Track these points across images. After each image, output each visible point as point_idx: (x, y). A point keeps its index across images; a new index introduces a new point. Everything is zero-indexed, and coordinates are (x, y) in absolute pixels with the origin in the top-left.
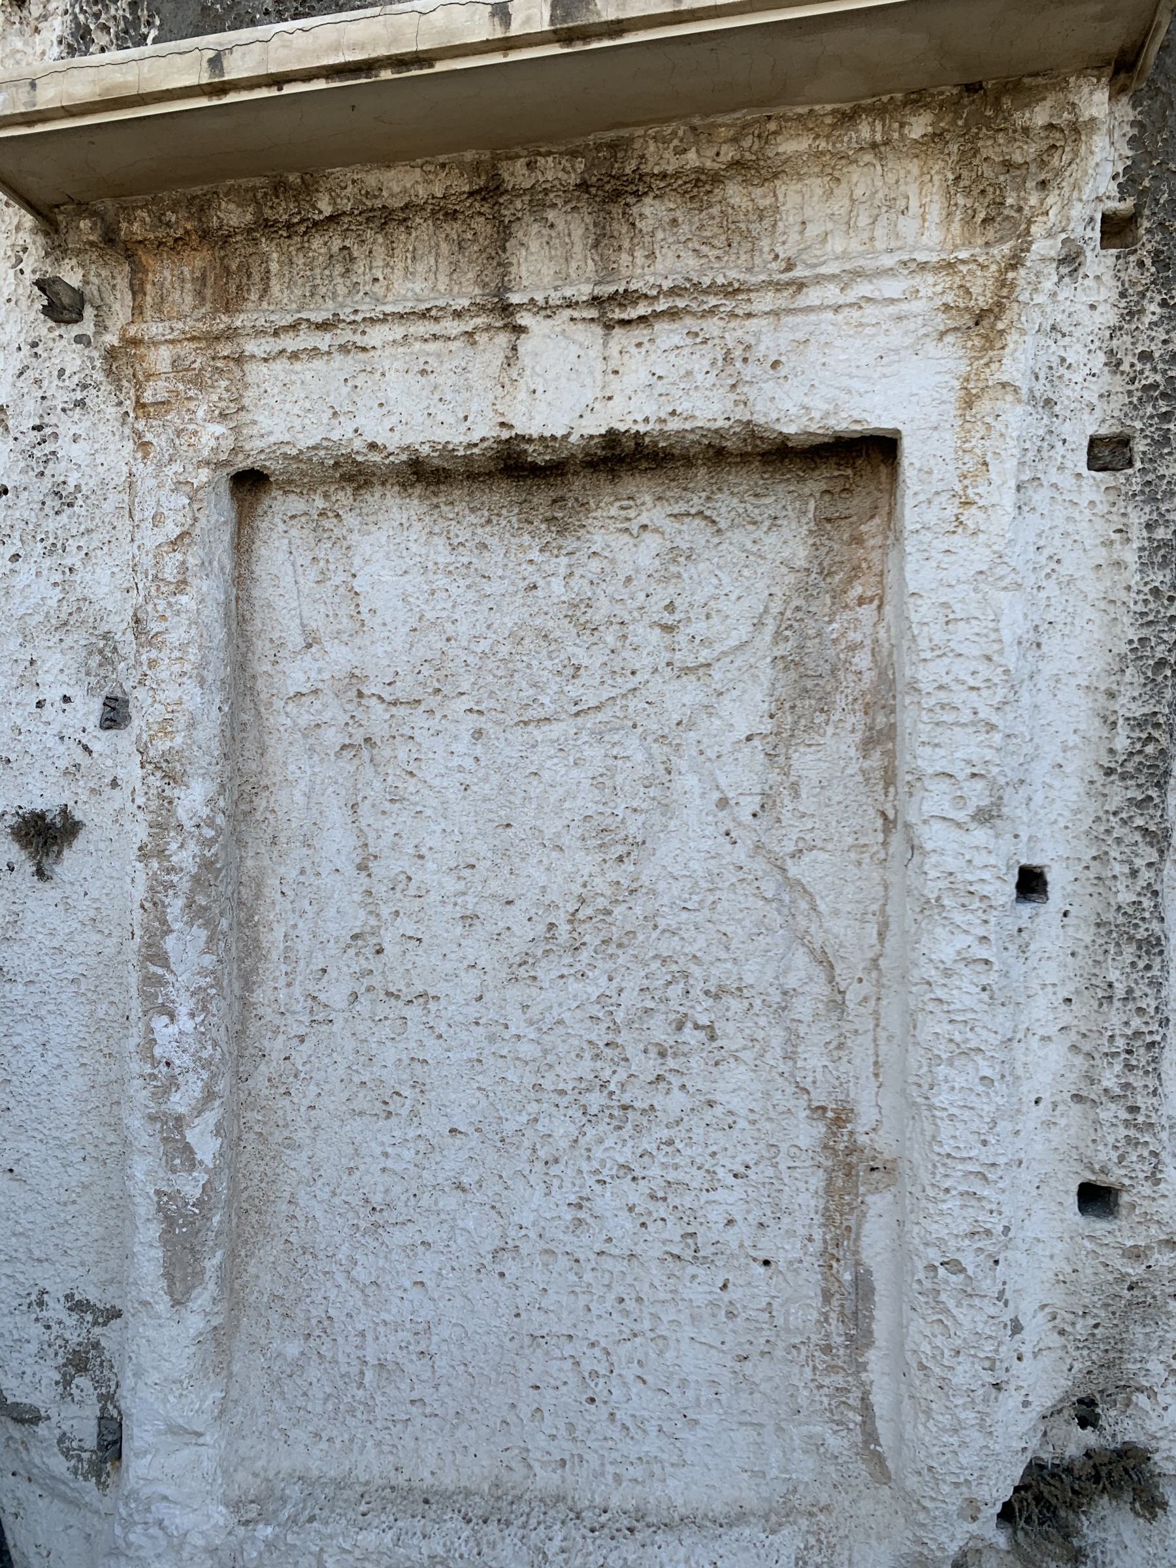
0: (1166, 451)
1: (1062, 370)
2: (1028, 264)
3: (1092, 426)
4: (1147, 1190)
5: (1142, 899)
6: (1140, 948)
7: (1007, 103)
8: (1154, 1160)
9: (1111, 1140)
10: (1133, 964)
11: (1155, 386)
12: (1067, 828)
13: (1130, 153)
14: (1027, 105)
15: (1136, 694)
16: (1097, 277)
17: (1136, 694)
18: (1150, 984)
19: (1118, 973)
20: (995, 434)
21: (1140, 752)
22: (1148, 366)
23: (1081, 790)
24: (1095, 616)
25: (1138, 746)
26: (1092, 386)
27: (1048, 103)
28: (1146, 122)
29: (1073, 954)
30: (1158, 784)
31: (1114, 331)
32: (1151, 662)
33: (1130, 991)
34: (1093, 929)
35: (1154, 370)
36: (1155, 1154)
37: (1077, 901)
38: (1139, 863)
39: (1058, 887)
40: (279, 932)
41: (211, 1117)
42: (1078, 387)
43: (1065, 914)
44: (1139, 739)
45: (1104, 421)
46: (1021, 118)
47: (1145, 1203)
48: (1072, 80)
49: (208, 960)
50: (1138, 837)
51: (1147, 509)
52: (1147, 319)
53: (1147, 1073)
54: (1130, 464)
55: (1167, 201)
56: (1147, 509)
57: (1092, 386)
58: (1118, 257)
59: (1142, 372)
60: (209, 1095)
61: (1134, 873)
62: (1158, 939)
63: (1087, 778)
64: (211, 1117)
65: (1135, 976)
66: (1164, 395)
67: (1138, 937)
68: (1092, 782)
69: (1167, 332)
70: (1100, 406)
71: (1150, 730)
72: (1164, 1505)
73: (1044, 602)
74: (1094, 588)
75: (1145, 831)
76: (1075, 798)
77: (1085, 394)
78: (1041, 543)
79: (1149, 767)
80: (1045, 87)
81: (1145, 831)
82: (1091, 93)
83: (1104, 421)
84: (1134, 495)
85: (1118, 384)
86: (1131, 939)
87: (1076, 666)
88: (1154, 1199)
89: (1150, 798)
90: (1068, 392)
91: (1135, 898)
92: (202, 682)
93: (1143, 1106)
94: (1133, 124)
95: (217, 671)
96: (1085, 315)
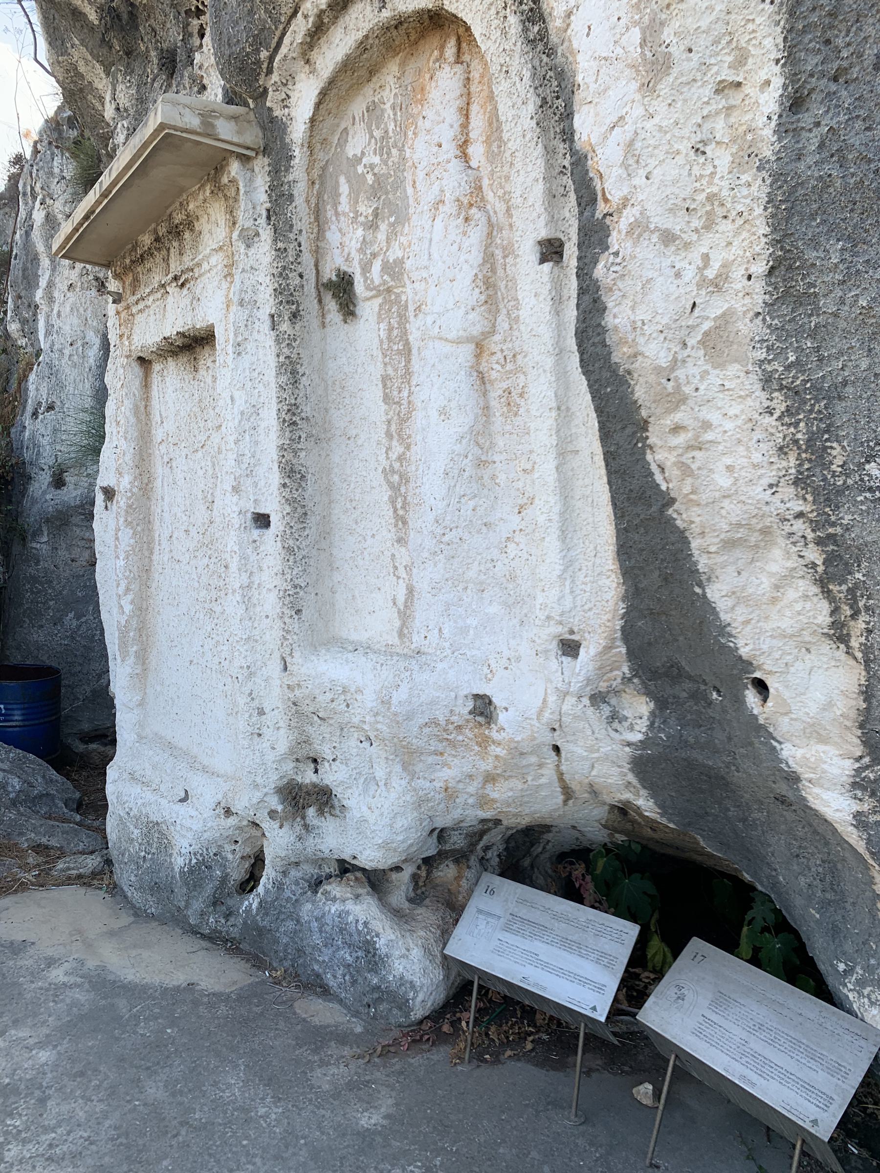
30: (289, 476)
40: (158, 533)
41: (130, 597)
49: (132, 541)
60: (128, 590)
64: (130, 597)
72: (279, 791)
73: (257, 395)
92: (126, 438)
94: (269, 165)
95: (133, 433)
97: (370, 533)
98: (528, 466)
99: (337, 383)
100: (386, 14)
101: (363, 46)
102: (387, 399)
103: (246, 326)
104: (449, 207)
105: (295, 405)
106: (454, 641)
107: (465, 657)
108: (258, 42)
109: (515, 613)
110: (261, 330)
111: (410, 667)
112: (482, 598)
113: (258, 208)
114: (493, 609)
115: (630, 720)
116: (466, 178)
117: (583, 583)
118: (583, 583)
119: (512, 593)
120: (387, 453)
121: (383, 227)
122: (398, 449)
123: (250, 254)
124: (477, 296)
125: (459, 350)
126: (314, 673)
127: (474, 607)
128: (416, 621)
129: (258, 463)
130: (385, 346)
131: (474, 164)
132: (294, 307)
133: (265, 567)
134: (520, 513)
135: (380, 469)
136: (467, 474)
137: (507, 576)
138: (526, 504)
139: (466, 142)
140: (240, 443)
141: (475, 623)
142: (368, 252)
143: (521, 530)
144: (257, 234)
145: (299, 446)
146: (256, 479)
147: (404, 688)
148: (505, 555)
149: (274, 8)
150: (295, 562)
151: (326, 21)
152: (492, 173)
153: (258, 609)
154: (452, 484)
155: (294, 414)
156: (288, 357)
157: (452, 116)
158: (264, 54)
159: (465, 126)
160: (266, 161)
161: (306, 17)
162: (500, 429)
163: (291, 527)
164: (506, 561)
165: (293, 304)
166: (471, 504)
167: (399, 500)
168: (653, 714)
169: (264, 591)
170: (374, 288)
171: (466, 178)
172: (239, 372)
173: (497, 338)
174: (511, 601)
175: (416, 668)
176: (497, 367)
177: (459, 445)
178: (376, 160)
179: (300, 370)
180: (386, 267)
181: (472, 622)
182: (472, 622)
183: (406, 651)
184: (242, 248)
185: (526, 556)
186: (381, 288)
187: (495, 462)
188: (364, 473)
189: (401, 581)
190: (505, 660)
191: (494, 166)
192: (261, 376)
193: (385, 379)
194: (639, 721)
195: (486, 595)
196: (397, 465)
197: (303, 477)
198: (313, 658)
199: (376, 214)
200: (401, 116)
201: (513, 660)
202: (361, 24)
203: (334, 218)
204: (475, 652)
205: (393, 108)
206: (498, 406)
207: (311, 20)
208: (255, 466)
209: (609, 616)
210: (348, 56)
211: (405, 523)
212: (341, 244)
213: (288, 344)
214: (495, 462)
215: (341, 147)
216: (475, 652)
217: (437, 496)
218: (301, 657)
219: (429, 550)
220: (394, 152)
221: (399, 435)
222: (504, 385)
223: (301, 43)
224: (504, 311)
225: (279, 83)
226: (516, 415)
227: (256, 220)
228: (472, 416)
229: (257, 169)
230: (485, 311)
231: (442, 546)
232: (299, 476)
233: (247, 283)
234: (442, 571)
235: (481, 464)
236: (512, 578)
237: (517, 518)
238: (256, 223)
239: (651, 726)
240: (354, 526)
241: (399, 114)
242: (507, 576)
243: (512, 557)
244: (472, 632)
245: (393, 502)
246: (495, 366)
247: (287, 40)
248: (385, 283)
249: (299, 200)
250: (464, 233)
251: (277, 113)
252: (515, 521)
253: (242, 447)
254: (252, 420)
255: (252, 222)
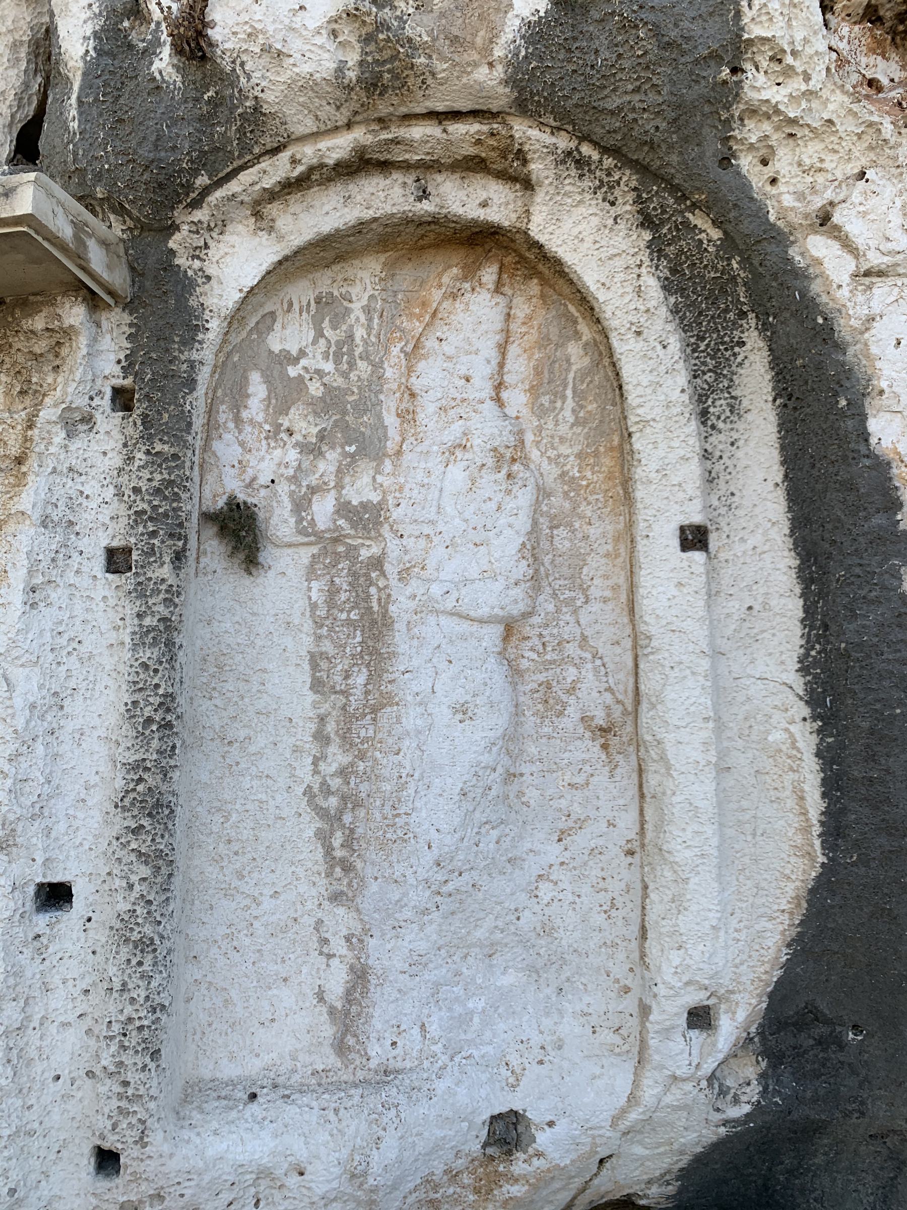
0: (152, 559)
1: (80, 500)
2: (39, 425)
3: (104, 540)
4: (135, 1152)
5: (137, 908)
6: (136, 947)
7: (18, 313)
8: (141, 1127)
9: (106, 1110)
10: (129, 961)
11: (144, 512)
12: (91, 849)
13: (129, 346)
14: (30, 315)
15: (130, 745)
16: (107, 432)
17: (130, 745)
18: (142, 977)
19: (115, 969)
20: (13, 550)
21: (134, 790)
22: (139, 498)
23: (100, 819)
24: (110, 683)
25: (132, 786)
26: (105, 511)
27: (43, 314)
28: (141, 323)
29: (94, 953)
30: (150, 815)
31: (120, 470)
32: (141, 720)
33: (124, 984)
34: (107, 932)
35: (143, 500)
36: (142, 1122)
37: (98, 909)
38: (134, 878)
39: (82, 898)
42: (93, 512)
43: (89, 920)
44: (133, 780)
45: (114, 536)
46: (27, 324)
47: (134, 1164)
48: (59, 298)
50: (133, 857)
51: (138, 603)
52: (137, 463)
53: (137, 1052)
54: (131, 568)
55: (150, 380)
56: (138, 603)
57: (105, 511)
58: (123, 419)
59: (135, 501)
61: (131, 887)
62: (152, 939)
63: (104, 810)
65: (128, 971)
66: (151, 519)
67: (133, 939)
68: (107, 813)
69: (151, 473)
70: (112, 525)
71: (141, 773)
73: (64, 674)
74: (108, 662)
75: (140, 854)
76: (96, 825)
77: (100, 517)
78: (61, 629)
79: (141, 802)
80: (42, 302)
81: (140, 854)
82: (71, 308)
83: (114, 536)
84: (130, 593)
85: (122, 510)
86: (127, 940)
87: (97, 722)
88: (142, 1160)
89: (142, 826)
90: (86, 516)
91: (129, 907)
93: (132, 1081)
94: (131, 325)
96: (99, 460)
97: (268, 891)
98: (580, 779)
99: (211, 659)
100: (427, 206)
101: (361, 227)
102: (317, 685)
103: (53, 560)
104: (479, 453)
105: (171, 695)
106: (449, 1040)
107: (473, 1061)
108: (201, 162)
109: (547, 979)
110: (84, 569)
111: (391, 1101)
112: (491, 966)
113: (99, 382)
114: (507, 980)
115: (733, 1091)
116: (510, 428)
117: (736, 930)
118: (736, 930)
119: (542, 951)
120: (315, 763)
121: (332, 456)
122: (337, 757)
123: (72, 448)
124: (522, 569)
125: (484, 631)
126: (201, 1164)
127: (479, 981)
128: (374, 1021)
129: (57, 792)
130: (322, 612)
131: (511, 411)
132: (180, 543)
133: (56, 980)
134: (560, 840)
135: (300, 790)
136: (493, 793)
137: (538, 929)
138: (571, 829)
139: (500, 384)
140: (21, 759)
141: (481, 1005)
142: (304, 484)
143: (562, 864)
144: (88, 420)
145: (172, 763)
146: (49, 822)
147: (390, 1141)
148: (536, 900)
149: (251, 132)
150: (155, 964)
151: (314, 177)
152: (540, 429)
153: (38, 1067)
154: (471, 809)
155: (168, 710)
156: (163, 620)
157: (488, 348)
158: (202, 180)
159: (501, 365)
160: (127, 318)
161: (294, 161)
162: (533, 732)
163: (149, 902)
164: (537, 908)
165: (179, 539)
166: (495, 834)
167: (339, 834)
168: (763, 1076)
169: (53, 1029)
170: (315, 534)
171: (510, 428)
172: (30, 636)
173: (536, 620)
174: (540, 963)
175: (402, 1099)
176: (534, 656)
177: (487, 755)
178: (329, 367)
179: (177, 640)
180: (344, 509)
181: (476, 1004)
182: (476, 1004)
183: (360, 1075)
184: (59, 436)
185: (571, 898)
186: (327, 535)
187: (522, 775)
188: (263, 797)
189: (335, 962)
190: (536, 1050)
191: (542, 421)
192: (75, 645)
193: (315, 660)
194: (748, 1090)
195: (497, 960)
196: (335, 783)
197: (172, 811)
198: (186, 1134)
199: (321, 436)
200: (380, 325)
201: (549, 1048)
202: (376, 203)
203: (231, 425)
204: (485, 1049)
205: (367, 310)
206: (530, 702)
207: (300, 169)
208: (50, 797)
209: (767, 967)
210: (337, 230)
211: (348, 868)
212: (240, 462)
213: (165, 600)
214: (522, 775)
215: (260, 334)
216: (485, 1049)
217: (444, 827)
218: (165, 1139)
219: (415, 907)
220: (362, 365)
221: (344, 738)
222: (541, 677)
223: (264, 189)
224: (548, 590)
225: (205, 226)
226: (560, 714)
227: (91, 399)
228: (506, 716)
229: (105, 325)
230: (529, 588)
231: (438, 898)
232: (167, 812)
233: (59, 492)
234: (434, 937)
235: (511, 776)
236: (547, 930)
237: (557, 848)
238: (94, 404)
239: (764, 1092)
240: (235, 883)
241: (376, 321)
242: (538, 929)
243: (545, 902)
244: (476, 1020)
245: (324, 837)
246: (528, 654)
247: (245, 177)
248: (338, 528)
249: (201, 390)
250: (509, 492)
251: (181, 261)
252: (553, 852)
253: (24, 766)
254: (49, 718)
255: (87, 401)
